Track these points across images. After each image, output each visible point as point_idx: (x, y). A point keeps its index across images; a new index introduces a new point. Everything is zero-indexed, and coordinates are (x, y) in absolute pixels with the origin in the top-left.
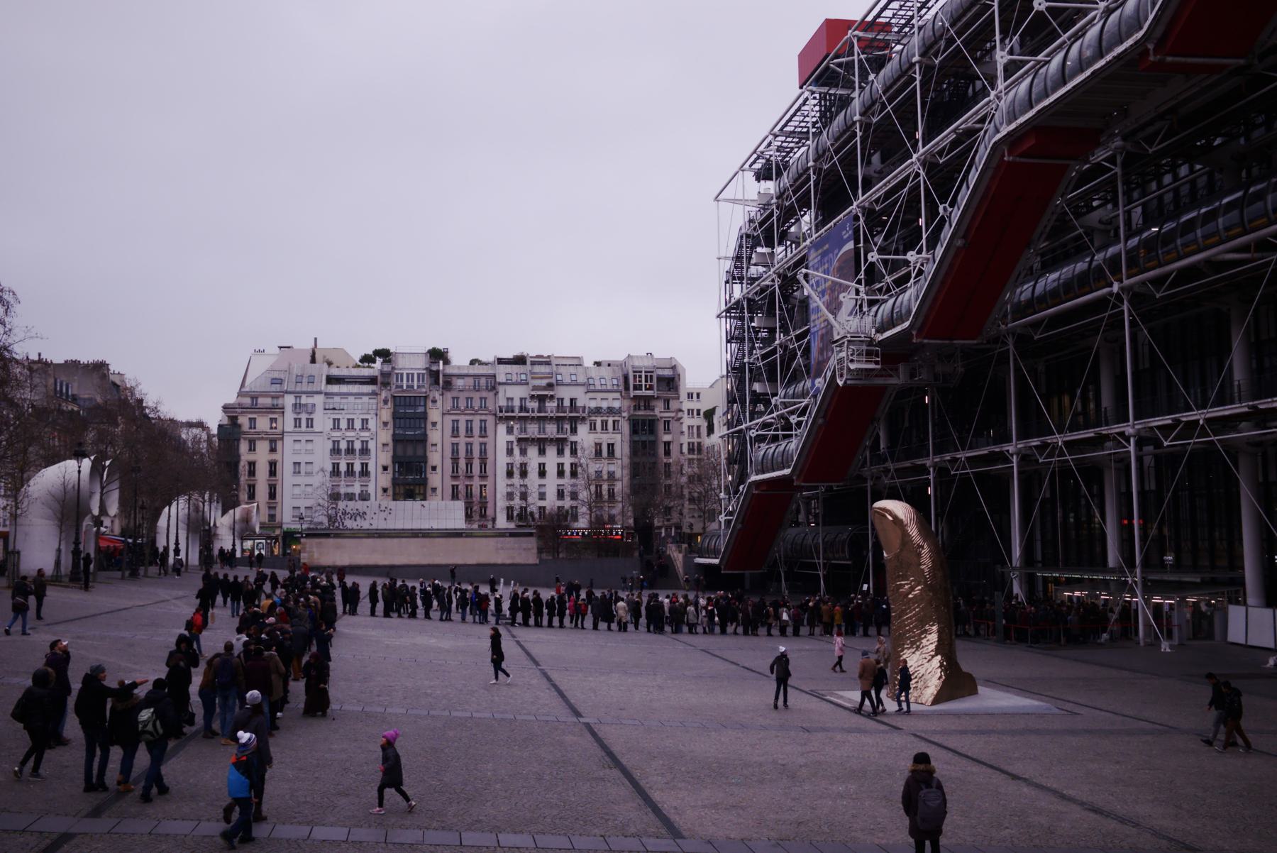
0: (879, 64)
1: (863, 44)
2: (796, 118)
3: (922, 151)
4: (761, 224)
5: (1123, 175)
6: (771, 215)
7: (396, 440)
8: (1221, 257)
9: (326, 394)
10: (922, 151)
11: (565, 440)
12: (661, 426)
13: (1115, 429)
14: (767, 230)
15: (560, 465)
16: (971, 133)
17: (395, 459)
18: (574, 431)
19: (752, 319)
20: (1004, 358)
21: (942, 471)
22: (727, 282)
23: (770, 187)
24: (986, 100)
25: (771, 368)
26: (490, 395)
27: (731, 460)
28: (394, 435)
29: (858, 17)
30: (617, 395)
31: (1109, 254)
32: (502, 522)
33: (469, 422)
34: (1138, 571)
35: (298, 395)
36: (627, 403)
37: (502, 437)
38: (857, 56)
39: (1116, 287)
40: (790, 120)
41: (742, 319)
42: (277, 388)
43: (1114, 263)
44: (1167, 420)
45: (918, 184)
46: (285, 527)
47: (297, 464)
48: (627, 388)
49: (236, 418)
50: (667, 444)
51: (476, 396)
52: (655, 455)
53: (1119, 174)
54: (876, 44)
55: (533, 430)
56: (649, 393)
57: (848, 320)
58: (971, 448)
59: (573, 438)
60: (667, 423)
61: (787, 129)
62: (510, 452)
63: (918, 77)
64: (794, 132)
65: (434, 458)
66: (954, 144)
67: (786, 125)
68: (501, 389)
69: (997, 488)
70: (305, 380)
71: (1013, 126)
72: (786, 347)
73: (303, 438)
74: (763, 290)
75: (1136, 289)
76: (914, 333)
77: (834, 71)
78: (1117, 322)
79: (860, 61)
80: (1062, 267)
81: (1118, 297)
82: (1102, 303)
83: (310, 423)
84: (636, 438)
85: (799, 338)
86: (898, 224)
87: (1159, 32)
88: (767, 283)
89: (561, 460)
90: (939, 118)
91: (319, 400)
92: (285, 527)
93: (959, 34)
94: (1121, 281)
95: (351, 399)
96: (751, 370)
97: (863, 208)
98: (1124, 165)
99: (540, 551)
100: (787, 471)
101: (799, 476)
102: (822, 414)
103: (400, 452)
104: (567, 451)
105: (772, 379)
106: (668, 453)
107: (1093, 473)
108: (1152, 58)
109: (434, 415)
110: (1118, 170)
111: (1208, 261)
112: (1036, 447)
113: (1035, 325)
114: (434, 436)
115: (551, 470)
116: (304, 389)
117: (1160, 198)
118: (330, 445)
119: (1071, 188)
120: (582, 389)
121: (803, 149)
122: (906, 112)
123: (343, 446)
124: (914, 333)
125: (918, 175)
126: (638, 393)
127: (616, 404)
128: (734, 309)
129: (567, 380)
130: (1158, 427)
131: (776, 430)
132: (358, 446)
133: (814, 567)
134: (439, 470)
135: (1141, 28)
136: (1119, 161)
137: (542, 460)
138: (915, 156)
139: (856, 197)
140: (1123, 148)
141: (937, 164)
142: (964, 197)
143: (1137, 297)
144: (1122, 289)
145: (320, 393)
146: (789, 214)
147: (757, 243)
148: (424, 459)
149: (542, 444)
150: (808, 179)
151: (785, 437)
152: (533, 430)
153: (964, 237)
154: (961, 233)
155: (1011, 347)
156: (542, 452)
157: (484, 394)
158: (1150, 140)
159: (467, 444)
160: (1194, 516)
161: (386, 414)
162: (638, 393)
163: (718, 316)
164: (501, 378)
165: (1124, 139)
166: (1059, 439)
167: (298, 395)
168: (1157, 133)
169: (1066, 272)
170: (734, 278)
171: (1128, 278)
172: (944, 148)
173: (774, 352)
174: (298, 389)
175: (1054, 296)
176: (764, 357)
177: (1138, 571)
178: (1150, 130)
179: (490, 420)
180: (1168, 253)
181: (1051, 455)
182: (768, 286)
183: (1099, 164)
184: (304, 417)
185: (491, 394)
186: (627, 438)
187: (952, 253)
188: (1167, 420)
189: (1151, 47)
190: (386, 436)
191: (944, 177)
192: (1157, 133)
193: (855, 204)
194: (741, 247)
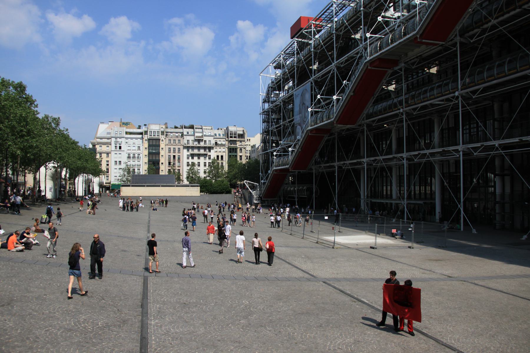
0: (319, 32)
4: (276, 83)
5: (404, 74)
6: (280, 80)
7: (150, 154)
8: (435, 103)
11: (207, 154)
12: (238, 150)
13: (399, 155)
14: (277, 85)
15: (205, 163)
17: (149, 161)
18: (210, 151)
19: (272, 115)
20: (363, 132)
21: (340, 167)
23: (279, 72)
26: (181, 139)
27: (264, 162)
28: (149, 152)
29: (314, 17)
31: (399, 99)
32: (186, 182)
33: (174, 148)
34: (405, 200)
35: (116, 138)
36: (227, 142)
38: (313, 29)
39: (401, 110)
40: (288, 49)
41: (269, 115)
42: (109, 136)
43: (401, 103)
44: (416, 153)
45: (334, 73)
46: (112, 183)
47: (116, 162)
48: (228, 137)
49: (95, 146)
50: (241, 156)
51: (177, 139)
52: (236, 160)
55: (196, 151)
56: (235, 139)
57: (308, 118)
58: (351, 160)
59: (209, 154)
60: (241, 149)
62: (188, 158)
65: (162, 160)
66: (347, 61)
68: (185, 137)
69: (357, 173)
70: (118, 133)
71: (372, 57)
73: (118, 153)
74: (276, 106)
77: (304, 34)
82: (396, 115)
83: (120, 148)
85: (289, 122)
86: (326, 86)
87: (421, 32)
90: (342, 52)
92: (112, 183)
94: (403, 108)
95: (129, 139)
96: (272, 133)
98: (405, 71)
99: (201, 192)
100: (287, 166)
103: (151, 158)
104: (207, 158)
105: (279, 135)
106: (241, 159)
107: (390, 169)
109: (162, 145)
111: (431, 104)
113: (373, 121)
114: (162, 153)
115: (202, 164)
116: (118, 136)
121: (291, 59)
122: (330, 48)
123: (132, 155)
125: (334, 70)
126: (231, 139)
127: (224, 143)
130: (413, 155)
132: (136, 155)
133: (294, 198)
134: (164, 164)
135: (415, 30)
139: (312, 76)
142: (354, 79)
143: (408, 114)
146: (286, 81)
147: (275, 90)
149: (199, 156)
150: (294, 69)
151: (284, 155)
152: (196, 151)
153: (353, 92)
154: (352, 91)
155: (365, 128)
156: (199, 158)
157: (180, 139)
158: (413, 64)
161: (146, 145)
162: (231, 139)
163: (260, 114)
164: (185, 133)
165: (405, 63)
166: (381, 158)
167: (116, 138)
168: (415, 62)
169: (384, 104)
170: (265, 101)
173: (280, 126)
175: (380, 112)
176: (276, 128)
177: (405, 200)
178: (413, 61)
179: (182, 147)
181: (377, 163)
184: (118, 145)
186: (227, 154)
187: (349, 97)
188: (416, 153)
189: (418, 36)
190: (146, 152)
191: (344, 72)
192: (415, 62)
194: (269, 91)
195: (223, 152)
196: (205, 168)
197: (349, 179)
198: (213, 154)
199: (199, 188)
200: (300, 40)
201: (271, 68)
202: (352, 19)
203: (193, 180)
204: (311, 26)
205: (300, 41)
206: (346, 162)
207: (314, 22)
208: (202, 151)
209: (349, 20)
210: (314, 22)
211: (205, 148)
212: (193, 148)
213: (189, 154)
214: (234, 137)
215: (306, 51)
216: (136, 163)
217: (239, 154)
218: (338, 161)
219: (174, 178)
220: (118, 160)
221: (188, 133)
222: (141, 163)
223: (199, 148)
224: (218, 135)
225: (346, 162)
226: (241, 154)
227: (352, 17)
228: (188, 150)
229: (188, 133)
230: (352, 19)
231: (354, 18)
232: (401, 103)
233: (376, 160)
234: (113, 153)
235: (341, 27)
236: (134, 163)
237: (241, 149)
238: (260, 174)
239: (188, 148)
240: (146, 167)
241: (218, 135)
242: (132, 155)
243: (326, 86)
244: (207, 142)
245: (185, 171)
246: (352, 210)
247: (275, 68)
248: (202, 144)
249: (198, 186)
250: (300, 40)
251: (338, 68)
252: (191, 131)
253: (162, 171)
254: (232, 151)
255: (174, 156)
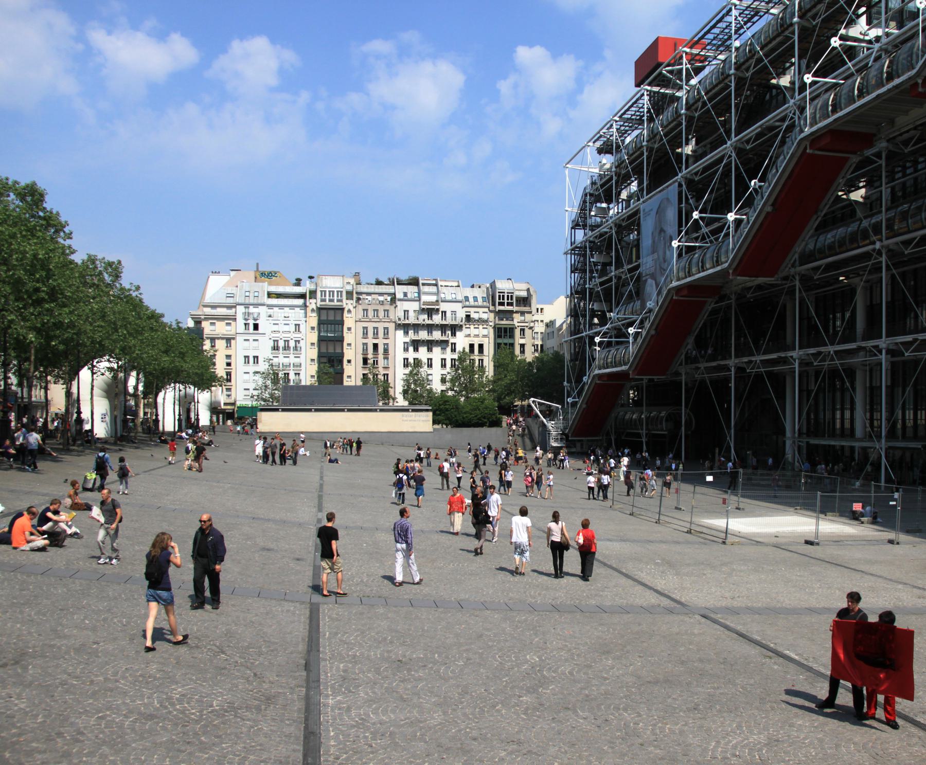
0: (698, 71)
1: (690, 57)
2: (633, 109)
3: (734, 140)
4: (602, 186)
5: (887, 165)
7: (321, 340)
9: (268, 306)
10: (734, 140)
11: (447, 342)
12: (517, 332)
13: (871, 343)
14: (604, 190)
15: (443, 360)
16: (771, 128)
17: (320, 356)
18: (454, 334)
19: (592, 256)
20: (792, 291)
21: (740, 370)
22: (572, 228)
23: (608, 161)
24: (786, 106)
25: (607, 293)
29: (689, 38)
30: (486, 310)
31: (873, 221)
32: (401, 402)
33: (376, 328)
35: (247, 306)
37: (400, 338)
38: (685, 65)
39: (878, 245)
40: (628, 110)
41: (585, 256)
42: (230, 301)
43: (877, 229)
44: (909, 338)
45: (730, 162)
46: (238, 404)
47: (247, 357)
48: (494, 305)
49: (200, 322)
50: (522, 346)
51: (381, 309)
52: (513, 353)
53: (884, 165)
54: (697, 58)
55: (423, 335)
56: (510, 308)
57: (670, 261)
59: (452, 340)
60: (523, 330)
61: (625, 116)
62: (406, 350)
63: (733, 85)
64: (630, 119)
65: (348, 354)
66: (759, 136)
67: (624, 113)
68: (398, 303)
69: (779, 382)
70: (252, 295)
71: (815, 128)
72: (620, 278)
73: (251, 338)
74: (601, 235)
75: (891, 247)
76: (731, 271)
77: (664, 76)
78: (877, 269)
79: (687, 69)
80: (838, 228)
81: (879, 253)
82: (867, 256)
83: (256, 327)
84: (500, 341)
85: (630, 271)
86: (713, 192)
88: (605, 230)
89: (443, 356)
91: (263, 310)
92: (238, 404)
93: (766, 55)
94: (881, 240)
95: (276, 309)
97: (686, 178)
98: (887, 158)
100: (624, 368)
101: (634, 371)
102: (654, 327)
103: (324, 350)
104: (449, 349)
105: (608, 300)
106: (523, 352)
107: (851, 373)
108: (920, 90)
110: (883, 162)
112: (812, 354)
114: (348, 338)
115: (437, 363)
116: (252, 301)
117: (904, 184)
118: (272, 344)
119: (850, 172)
120: (460, 305)
121: (636, 132)
123: (281, 344)
124: (731, 271)
125: (730, 156)
126: (502, 308)
127: (485, 316)
128: (578, 250)
129: (449, 298)
130: (902, 343)
131: (611, 337)
132: (292, 344)
136: (884, 157)
137: (430, 356)
138: (729, 143)
140: (887, 148)
141: (745, 150)
142: (774, 177)
143: (891, 253)
144: (882, 247)
145: (263, 305)
146: (623, 180)
147: (598, 199)
148: (342, 355)
149: (430, 344)
150: (642, 154)
151: (618, 343)
152: (423, 335)
153: (773, 205)
154: (771, 202)
155: (797, 283)
157: (387, 307)
159: (385, 344)
160: (5, 221)
162: (502, 308)
163: (566, 253)
164: (399, 295)
165: (888, 141)
166: (831, 349)
167: (247, 306)
169: (841, 232)
171: (887, 239)
172: (750, 139)
173: (610, 280)
174: (247, 302)
175: (831, 249)
176: (602, 284)
178: (906, 136)
179: (392, 326)
180: (915, 223)
182: (606, 233)
183: (867, 157)
184: (251, 322)
185: (392, 307)
188: (909, 338)
191: (753, 161)
192: (912, 139)
193: (680, 175)
194: (585, 202)
195: (484, 336)
196: (444, 372)
197: (762, 394)
198: (461, 341)
199: (431, 414)
200: (656, 89)
201: (591, 152)
202: (774, 43)
203: (417, 396)
204: (681, 57)
205: (655, 92)
206: (753, 359)
207: (688, 50)
208: (437, 335)
209: (766, 45)
210: (688, 50)
211: (443, 328)
212: (417, 327)
213: (407, 340)
214: (509, 304)
215: (667, 115)
216: (292, 360)
217: (518, 340)
218: (736, 357)
219: (375, 393)
220: (251, 354)
221: (405, 294)
222: (302, 360)
223: (430, 328)
224: (471, 300)
225: (753, 359)
226: (522, 341)
227: (774, 38)
228: (406, 333)
229: (405, 294)
230: (774, 43)
231: (778, 39)
232: (877, 229)
233: (820, 353)
234: (240, 339)
235: (747, 60)
236: (286, 361)
237: (523, 330)
238: (565, 383)
239: (406, 328)
240: (313, 369)
241: (471, 300)
242: (281, 344)
243: (713, 192)
244: (449, 315)
245: (399, 378)
246: (767, 462)
247: (600, 151)
248: (437, 319)
249: (427, 410)
250: (656, 89)
251: (740, 151)
252: (412, 290)
253: (349, 377)
254: (504, 334)
255: (376, 346)
